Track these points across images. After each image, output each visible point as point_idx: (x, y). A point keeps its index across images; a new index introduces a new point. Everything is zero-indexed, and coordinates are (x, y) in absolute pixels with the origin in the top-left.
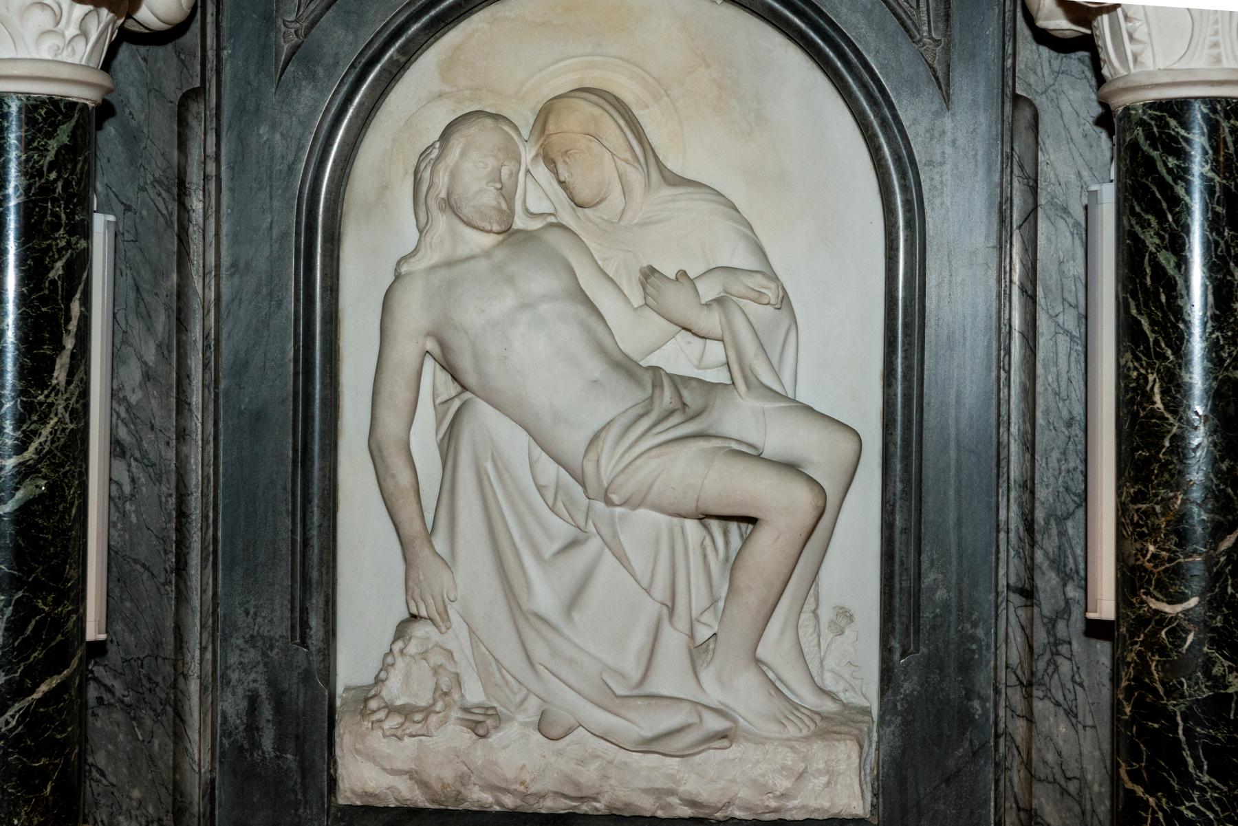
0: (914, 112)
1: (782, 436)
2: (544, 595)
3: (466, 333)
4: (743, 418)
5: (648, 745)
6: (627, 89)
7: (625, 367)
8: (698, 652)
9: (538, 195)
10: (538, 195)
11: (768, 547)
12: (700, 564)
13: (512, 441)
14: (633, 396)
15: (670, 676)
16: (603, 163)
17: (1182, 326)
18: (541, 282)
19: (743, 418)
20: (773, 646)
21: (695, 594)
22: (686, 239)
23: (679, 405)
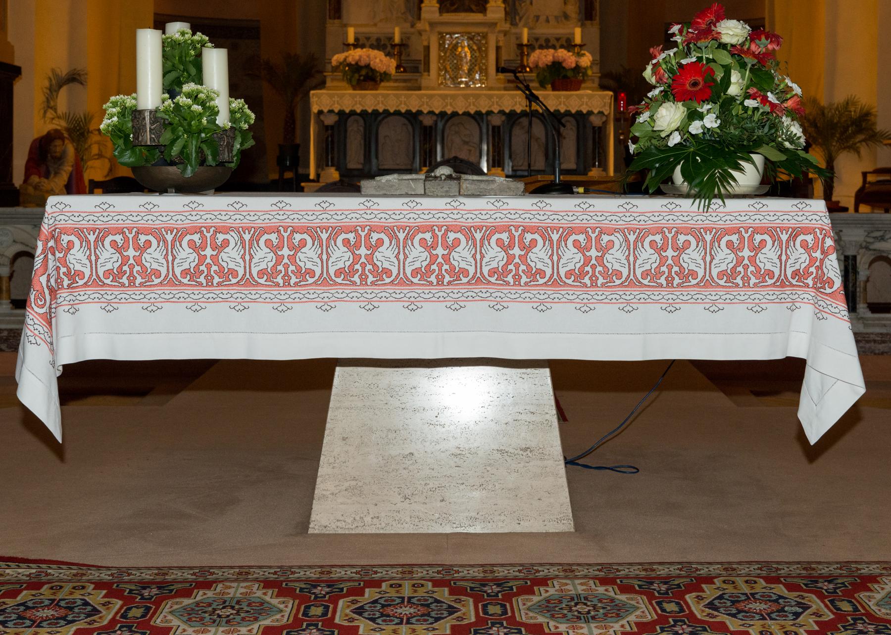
23: (466, 143)
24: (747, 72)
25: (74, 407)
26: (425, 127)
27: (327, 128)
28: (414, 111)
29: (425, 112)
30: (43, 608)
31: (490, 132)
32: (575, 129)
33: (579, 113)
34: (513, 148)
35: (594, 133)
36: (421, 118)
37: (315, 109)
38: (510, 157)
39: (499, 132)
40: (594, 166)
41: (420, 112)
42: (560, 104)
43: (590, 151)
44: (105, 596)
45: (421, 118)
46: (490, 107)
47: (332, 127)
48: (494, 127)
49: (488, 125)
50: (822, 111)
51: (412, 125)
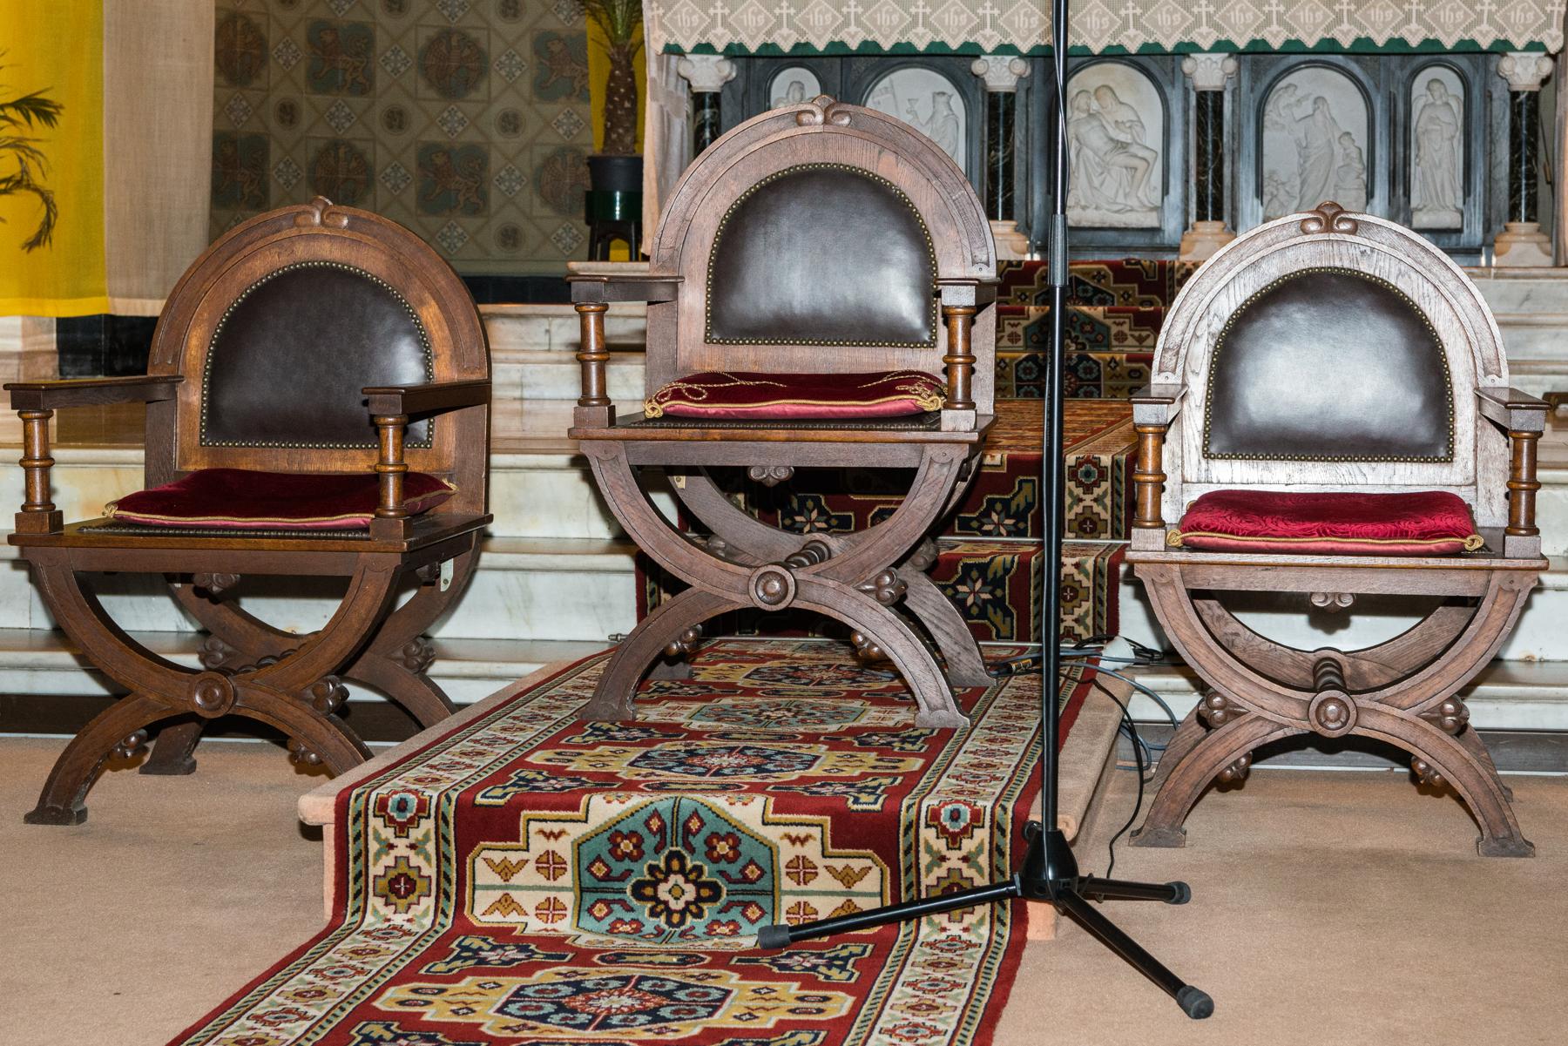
0: (1168, 90)
1: (1141, 153)
2: (1096, 183)
3: (1356, 867)
4: (1134, 149)
5: (1118, 212)
6: (1112, 85)
7: (1112, 139)
8: (1126, 195)
9: (1095, 106)
10: (1095, 106)
11: (1139, 174)
12: (602, 567)
13: (1090, 154)
14: (1111, 145)
15: (1120, 199)
16: (1108, 99)
17: (448, 570)
18: (1095, 123)
19: (1134, 149)
20: (1140, 194)
21: (1125, 183)
22: (1124, 115)
23: (1122, 146)
24: (1058, 283)
25: (424, 723)
26: (993, 98)
27: (699, 100)
28: (954, 45)
29: (989, 48)
30: (620, 1011)
31: (1192, 115)
32: (1457, 107)
33: (1468, 49)
34: (1267, 166)
35: (1515, 114)
36: (978, 67)
37: (655, 42)
38: (1259, 193)
39: (1218, 113)
40: (1513, 214)
41: (1186, 50)
42: (1407, 20)
43: (1503, 171)
44: (422, 1014)
45: (978, 67)
46: (1187, 31)
47: (716, 98)
48: (1202, 95)
49: (1186, 91)
50: (1320, 340)
51: (963, 94)
